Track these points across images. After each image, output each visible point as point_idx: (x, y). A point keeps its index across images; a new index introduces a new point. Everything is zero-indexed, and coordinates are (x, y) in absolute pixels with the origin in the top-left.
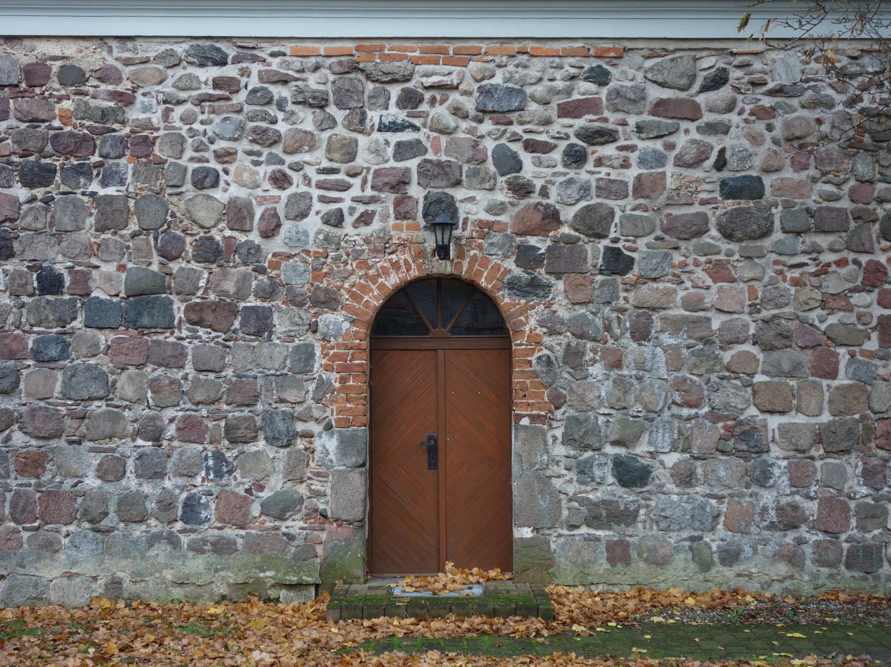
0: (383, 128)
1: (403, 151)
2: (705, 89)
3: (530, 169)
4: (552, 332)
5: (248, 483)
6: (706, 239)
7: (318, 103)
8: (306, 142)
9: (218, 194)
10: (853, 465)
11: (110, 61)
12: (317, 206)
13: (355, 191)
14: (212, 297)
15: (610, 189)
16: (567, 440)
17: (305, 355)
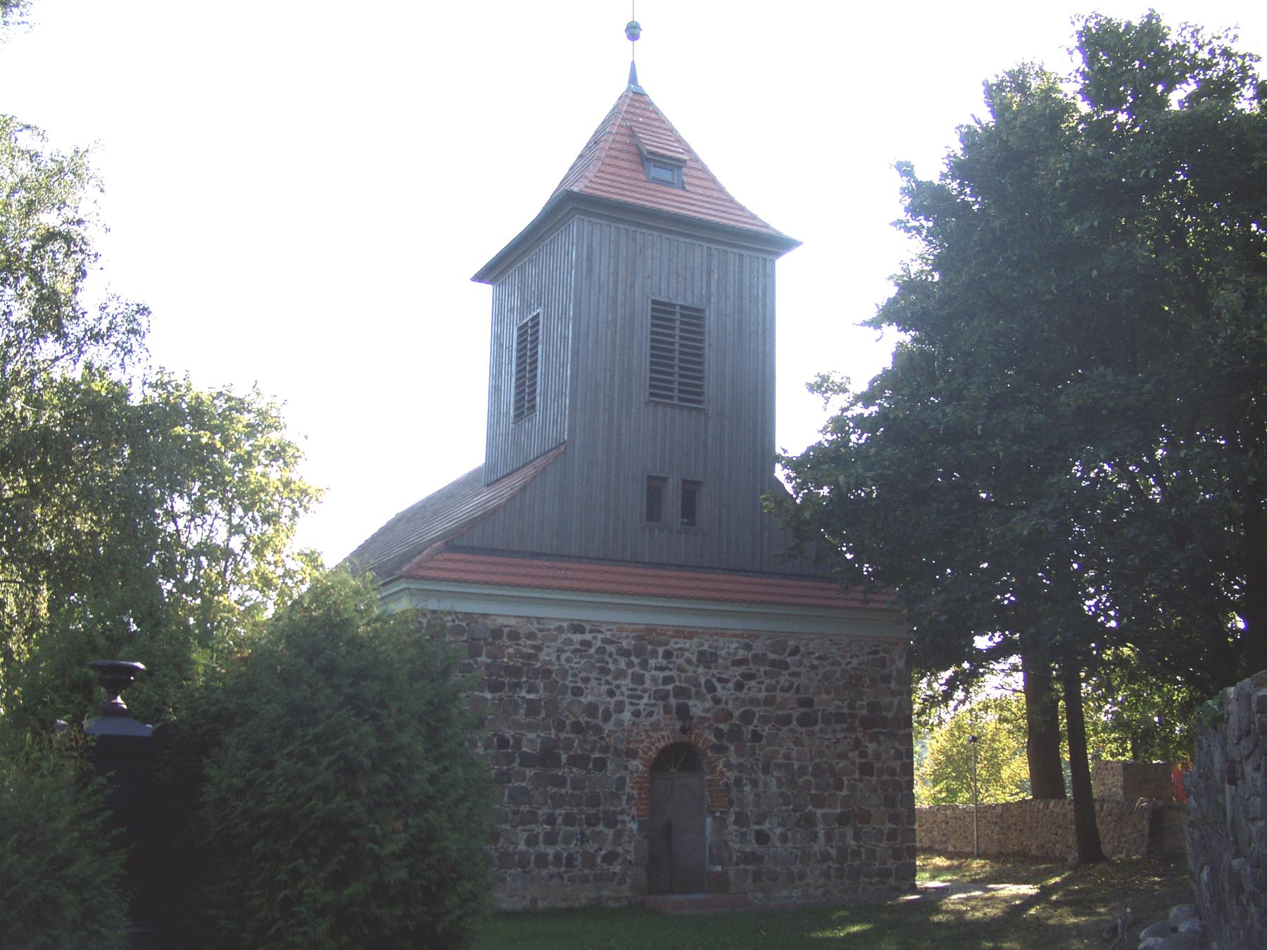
0: (656, 669)
1: (668, 680)
2: (790, 655)
3: (720, 692)
4: (730, 770)
5: (596, 846)
6: (791, 726)
7: (625, 653)
8: (621, 674)
9: (583, 699)
10: (849, 831)
11: (532, 629)
12: (628, 707)
13: (645, 700)
14: (579, 752)
15: (755, 702)
16: (736, 822)
17: (622, 781)
